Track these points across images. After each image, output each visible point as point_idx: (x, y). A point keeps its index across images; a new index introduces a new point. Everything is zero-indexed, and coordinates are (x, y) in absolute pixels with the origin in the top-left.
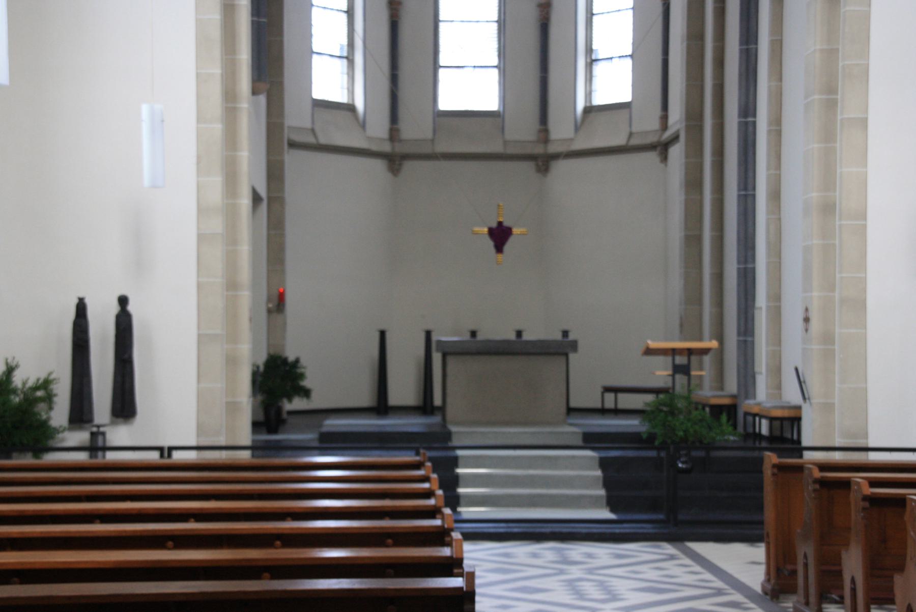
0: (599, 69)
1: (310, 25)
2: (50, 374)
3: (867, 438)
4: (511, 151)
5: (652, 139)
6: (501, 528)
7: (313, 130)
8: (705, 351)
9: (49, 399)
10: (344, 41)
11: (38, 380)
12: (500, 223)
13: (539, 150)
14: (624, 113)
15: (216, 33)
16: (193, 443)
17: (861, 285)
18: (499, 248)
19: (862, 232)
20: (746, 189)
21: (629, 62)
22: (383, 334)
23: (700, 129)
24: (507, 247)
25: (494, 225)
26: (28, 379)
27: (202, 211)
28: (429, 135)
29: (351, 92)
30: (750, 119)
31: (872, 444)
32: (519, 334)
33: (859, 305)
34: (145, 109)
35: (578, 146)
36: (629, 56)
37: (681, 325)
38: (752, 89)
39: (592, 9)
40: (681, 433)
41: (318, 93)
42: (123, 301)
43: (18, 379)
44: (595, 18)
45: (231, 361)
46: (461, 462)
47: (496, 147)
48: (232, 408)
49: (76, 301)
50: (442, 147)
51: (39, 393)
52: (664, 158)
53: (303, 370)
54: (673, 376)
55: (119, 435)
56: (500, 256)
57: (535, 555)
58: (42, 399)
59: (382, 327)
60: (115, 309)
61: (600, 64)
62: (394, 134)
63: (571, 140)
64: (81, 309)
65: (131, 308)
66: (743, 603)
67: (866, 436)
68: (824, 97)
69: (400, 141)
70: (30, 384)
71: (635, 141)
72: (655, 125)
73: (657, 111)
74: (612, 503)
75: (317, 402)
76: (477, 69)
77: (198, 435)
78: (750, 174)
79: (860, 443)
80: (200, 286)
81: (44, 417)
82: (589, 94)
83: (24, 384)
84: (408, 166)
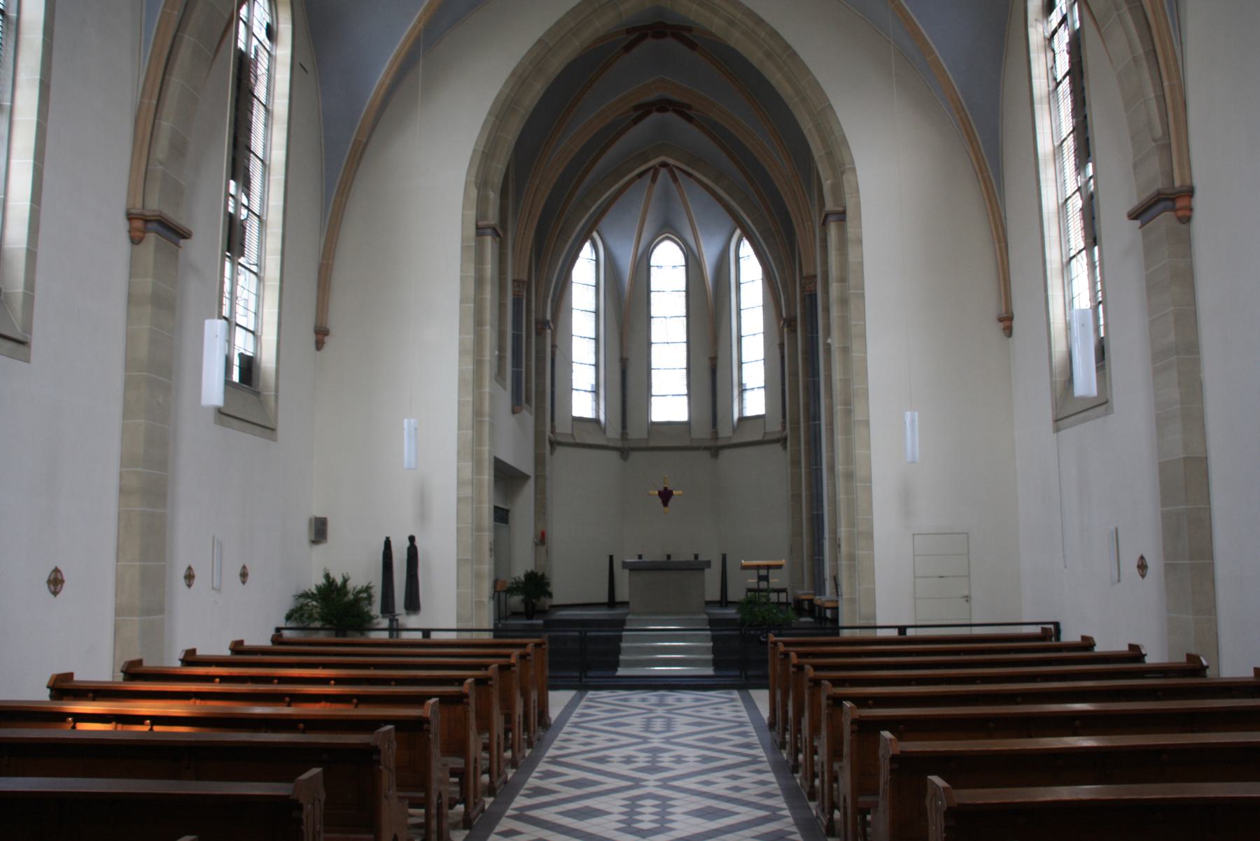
0: (747, 395)
1: (765, 373)
2: (370, 583)
3: (875, 619)
5: (778, 436)
6: (696, 681)
7: (572, 435)
8: (779, 567)
9: (370, 597)
10: (593, 382)
11: (362, 587)
12: (666, 488)
13: (712, 444)
15: (470, 376)
16: (454, 627)
17: (870, 523)
18: (665, 503)
19: (870, 489)
21: (763, 390)
23: (798, 429)
24: (671, 503)
25: (662, 489)
26: (357, 586)
27: (460, 483)
28: (646, 437)
30: (817, 422)
31: (879, 624)
32: (696, 557)
33: (870, 536)
34: (406, 421)
35: (734, 441)
39: (741, 360)
40: (760, 619)
42: (412, 539)
43: (351, 585)
44: (743, 365)
45: (478, 576)
46: (624, 639)
47: (686, 443)
48: (479, 604)
49: (384, 539)
50: (652, 444)
51: (365, 595)
53: (548, 581)
54: (758, 582)
55: (412, 621)
56: (666, 508)
57: (644, 700)
58: (365, 599)
59: (611, 554)
60: (407, 544)
61: (590, 389)
63: (730, 438)
64: (388, 544)
65: (418, 543)
66: (750, 732)
67: (874, 617)
68: (843, 407)
69: (628, 440)
70: (359, 587)
71: (768, 437)
72: (779, 428)
74: (716, 664)
75: (556, 600)
76: (674, 397)
77: (458, 622)
79: (871, 623)
80: (458, 530)
81: (366, 610)
82: (741, 410)
83: (355, 589)
84: (633, 455)
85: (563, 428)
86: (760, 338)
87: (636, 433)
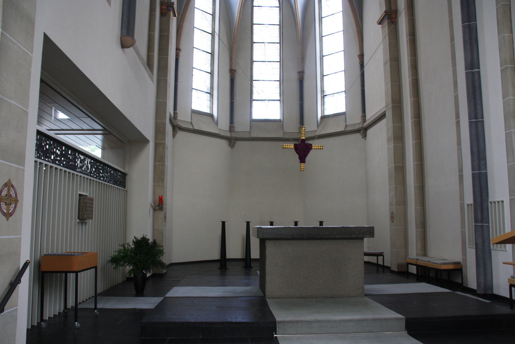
4: (286, 137)
7: (191, 122)
10: (209, 85)
14: (343, 117)
18: (302, 160)
20: (476, 118)
22: (223, 223)
28: (249, 130)
29: (212, 108)
36: (344, 91)
37: (392, 218)
38: (475, 52)
41: (195, 106)
47: (280, 135)
50: (254, 135)
52: (365, 136)
53: (161, 248)
62: (232, 128)
69: (235, 132)
71: (348, 129)
73: (360, 114)
78: (479, 107)
82: (323, 111)
84: (238, 144)
85: (183, 117)
86: (341, 57)
87: (241, 127)
